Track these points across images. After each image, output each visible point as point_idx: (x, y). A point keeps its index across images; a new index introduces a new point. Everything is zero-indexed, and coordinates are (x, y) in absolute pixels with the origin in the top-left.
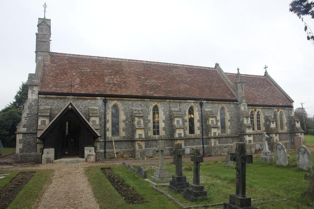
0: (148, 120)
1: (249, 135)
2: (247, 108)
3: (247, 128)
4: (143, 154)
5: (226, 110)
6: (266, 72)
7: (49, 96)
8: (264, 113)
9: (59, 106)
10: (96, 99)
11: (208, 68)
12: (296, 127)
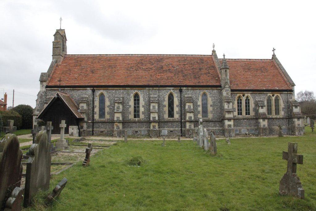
1: (229, 120)
2: (230, 94)
3: (227, 113)
5: (208, 95)
8: (254, 98)
9: (53, 95)
10: (86, 89)
12: (293, 113)
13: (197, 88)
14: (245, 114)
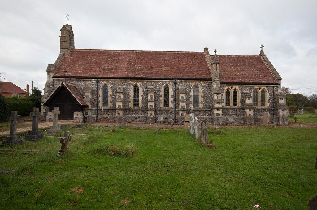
0: (129, 95)
1: (218, 109)
2: (219, 86)
3: (216, 103)
4: (120, 120)
6: (262, 52)
7: (60, 79)
8: (241, 90)
11: (197, 52)
12: (279, 104)
14: (232, 105)
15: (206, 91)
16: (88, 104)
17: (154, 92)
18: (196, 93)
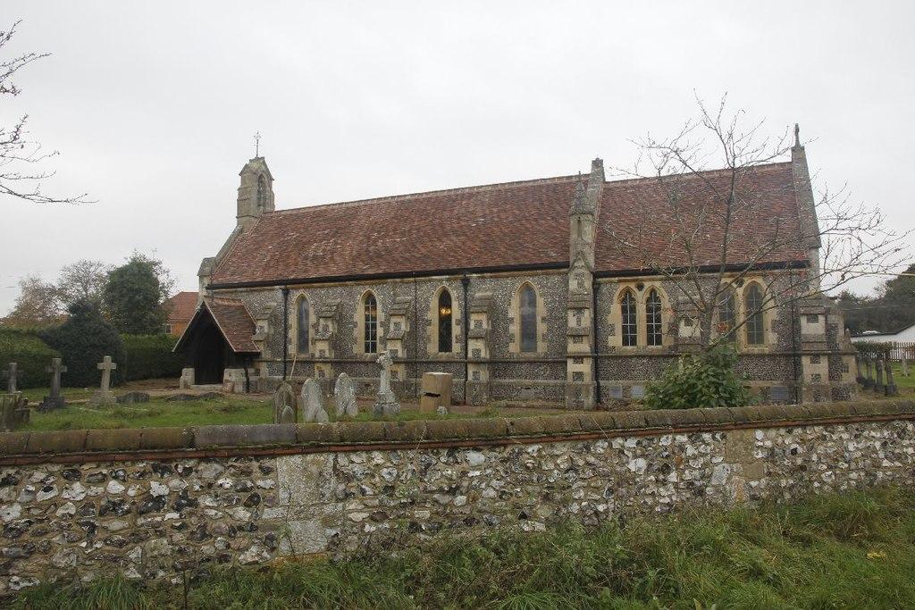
3: (570, 341)
13: (504, 274)
14: (645, 343)
15: (554, 301)
16: (260, 348)
17: (485, 309)
18: (371, 313)
